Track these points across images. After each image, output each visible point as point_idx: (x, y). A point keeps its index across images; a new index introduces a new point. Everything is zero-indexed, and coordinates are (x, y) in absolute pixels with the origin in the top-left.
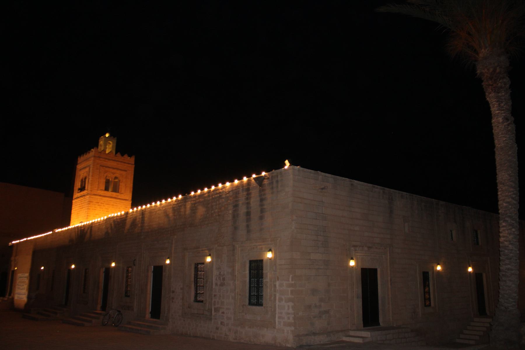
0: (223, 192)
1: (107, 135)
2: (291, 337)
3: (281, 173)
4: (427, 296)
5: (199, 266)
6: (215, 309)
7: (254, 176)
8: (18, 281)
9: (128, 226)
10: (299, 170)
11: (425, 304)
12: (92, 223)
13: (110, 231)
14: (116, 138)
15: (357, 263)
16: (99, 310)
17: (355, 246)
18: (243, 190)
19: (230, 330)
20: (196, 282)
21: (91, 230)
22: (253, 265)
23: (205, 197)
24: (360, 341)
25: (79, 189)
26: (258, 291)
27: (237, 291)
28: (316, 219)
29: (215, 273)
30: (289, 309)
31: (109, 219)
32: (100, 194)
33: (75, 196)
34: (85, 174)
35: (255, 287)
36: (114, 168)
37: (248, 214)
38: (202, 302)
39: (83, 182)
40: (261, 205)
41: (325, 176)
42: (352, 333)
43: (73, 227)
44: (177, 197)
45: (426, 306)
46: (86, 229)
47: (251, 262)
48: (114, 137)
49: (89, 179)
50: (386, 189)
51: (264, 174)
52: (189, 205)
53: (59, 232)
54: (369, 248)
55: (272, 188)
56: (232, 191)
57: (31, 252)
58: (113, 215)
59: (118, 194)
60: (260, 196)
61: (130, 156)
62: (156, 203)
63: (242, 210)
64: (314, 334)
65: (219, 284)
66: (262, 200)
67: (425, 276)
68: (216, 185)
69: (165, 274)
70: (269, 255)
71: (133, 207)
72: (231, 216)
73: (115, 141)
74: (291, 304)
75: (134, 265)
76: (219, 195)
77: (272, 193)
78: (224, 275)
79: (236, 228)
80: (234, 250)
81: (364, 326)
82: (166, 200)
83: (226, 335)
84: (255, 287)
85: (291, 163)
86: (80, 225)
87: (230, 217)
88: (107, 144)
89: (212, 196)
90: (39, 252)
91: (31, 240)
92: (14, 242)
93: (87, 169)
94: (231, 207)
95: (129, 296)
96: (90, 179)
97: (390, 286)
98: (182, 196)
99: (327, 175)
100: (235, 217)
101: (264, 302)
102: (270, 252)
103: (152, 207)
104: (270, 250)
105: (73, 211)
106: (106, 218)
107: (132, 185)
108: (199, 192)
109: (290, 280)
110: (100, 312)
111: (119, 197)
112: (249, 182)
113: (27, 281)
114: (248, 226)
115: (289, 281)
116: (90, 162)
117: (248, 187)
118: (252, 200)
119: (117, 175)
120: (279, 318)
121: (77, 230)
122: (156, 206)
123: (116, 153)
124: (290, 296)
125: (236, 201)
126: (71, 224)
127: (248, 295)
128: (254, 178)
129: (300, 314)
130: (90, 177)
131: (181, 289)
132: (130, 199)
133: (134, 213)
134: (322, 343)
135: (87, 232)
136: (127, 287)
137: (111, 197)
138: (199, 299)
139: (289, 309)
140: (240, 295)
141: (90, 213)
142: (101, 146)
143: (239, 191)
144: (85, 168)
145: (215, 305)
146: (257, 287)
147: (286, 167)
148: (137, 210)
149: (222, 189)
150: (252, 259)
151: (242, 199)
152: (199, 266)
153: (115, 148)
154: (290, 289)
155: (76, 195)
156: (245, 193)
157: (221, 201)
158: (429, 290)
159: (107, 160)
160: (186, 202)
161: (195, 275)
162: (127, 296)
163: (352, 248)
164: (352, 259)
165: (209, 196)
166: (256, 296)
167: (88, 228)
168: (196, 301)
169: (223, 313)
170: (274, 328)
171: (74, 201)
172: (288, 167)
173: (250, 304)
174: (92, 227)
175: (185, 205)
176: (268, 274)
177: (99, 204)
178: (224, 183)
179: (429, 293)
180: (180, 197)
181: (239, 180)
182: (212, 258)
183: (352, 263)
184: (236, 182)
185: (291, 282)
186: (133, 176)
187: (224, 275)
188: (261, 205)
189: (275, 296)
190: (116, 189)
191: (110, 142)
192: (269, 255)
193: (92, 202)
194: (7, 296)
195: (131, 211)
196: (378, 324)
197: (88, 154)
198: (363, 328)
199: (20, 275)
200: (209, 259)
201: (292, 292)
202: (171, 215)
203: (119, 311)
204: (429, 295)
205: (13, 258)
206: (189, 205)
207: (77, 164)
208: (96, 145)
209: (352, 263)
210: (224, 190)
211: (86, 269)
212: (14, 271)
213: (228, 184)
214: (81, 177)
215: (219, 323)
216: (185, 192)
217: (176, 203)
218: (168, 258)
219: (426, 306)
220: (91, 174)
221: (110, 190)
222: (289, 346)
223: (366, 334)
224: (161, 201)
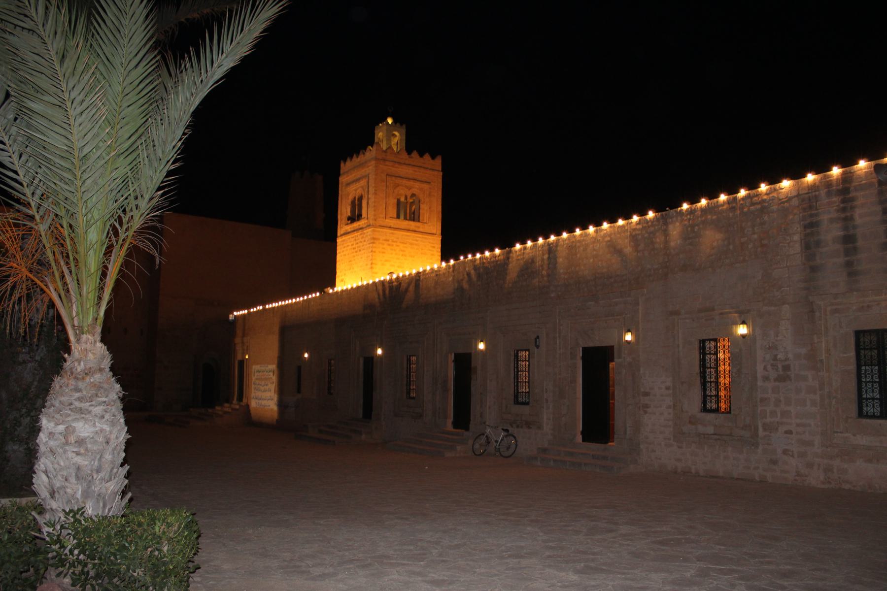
0: (773, 199)
6: (764, 425)
8: (254, 378)
12: (418, 273)
14: (404, 126)
18: (829, 194)
25: (349, 218)
32: (389, 225)
34: (359, 192)
36: (409, 179)
37: (849, 240)
46: (404, 285)
48: (401, 125)
56: (798, 195)
57: (276, 329)
59: (417, 224)
72: (797, 248)
73: (404, 131)
76: (763, 206)
80: (812, 311)
83: (798, 474)
88: (389, 135)
90: (291, 331)
93: (363, 183)
100: (810, 246)
111: (421, 230)
118: (857, 212)
119: (415, 191)
121: (380, 288)
125: (844, 210)
132: (440, 232)
133: (528, 251)
135: (407, 290)
137: (408, 230)
144: (358, 180)
149: (767, 194)
155: (342, 228)
159: (397, 165)
160: (666, 224)
165: (733, 209)
167: (409, 284)
177: (390, 242)
190: (414, 217)
191: (396, 133)
193: (378, 239)
194: (235, 401)
199: (256, 367)
202: (628, 250)
203: (507, 431)
205: (238, 340)
206: (675, 230)
208: (369, 140)
213: (786, 184)
214: (351, 197)
216: (666, 202)
220: (372, 190)
221: (402, 217)
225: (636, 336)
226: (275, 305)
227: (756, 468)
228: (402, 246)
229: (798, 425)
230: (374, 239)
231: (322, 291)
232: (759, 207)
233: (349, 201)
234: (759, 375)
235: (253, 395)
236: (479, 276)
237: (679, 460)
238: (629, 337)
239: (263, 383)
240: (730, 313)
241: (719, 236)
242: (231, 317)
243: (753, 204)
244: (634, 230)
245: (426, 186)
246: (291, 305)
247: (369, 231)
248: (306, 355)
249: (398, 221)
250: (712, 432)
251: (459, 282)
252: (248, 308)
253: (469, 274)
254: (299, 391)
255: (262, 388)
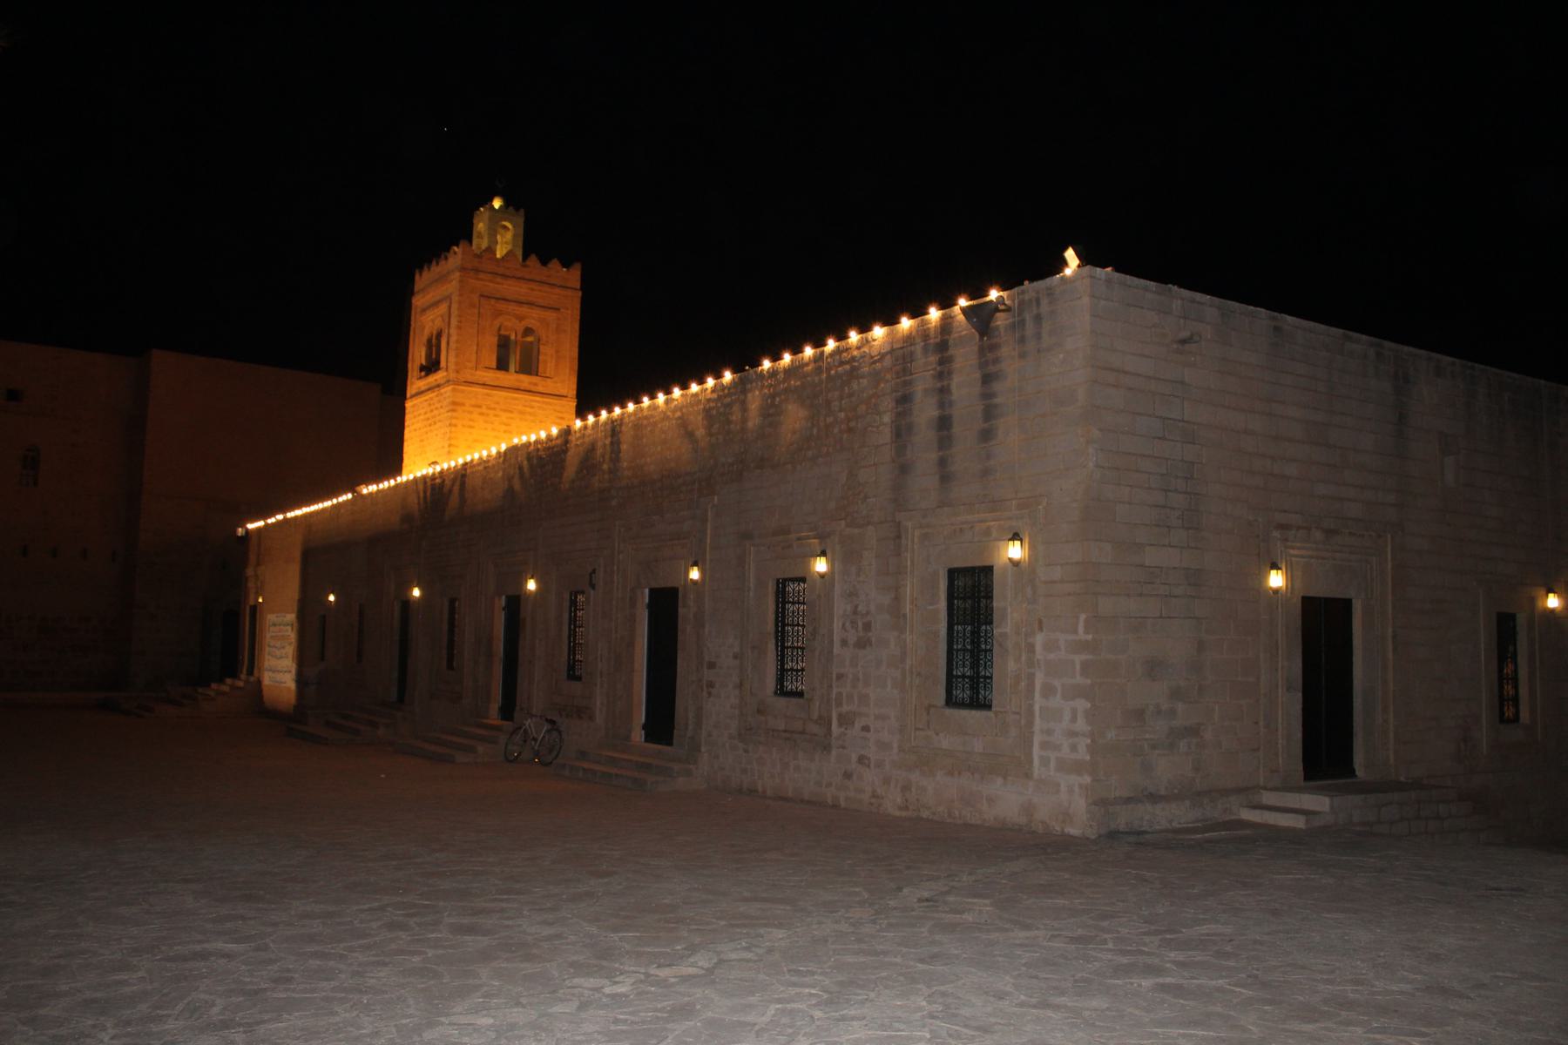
1: (497, 203)
2: (1080, 805)
3: (1050, 292)
4: (1509, 689)
5: (787, 591)
6: (840, 716)
7: (963, 302)
9: (571, 470)
10: (1109, 281)
11: (1502, 713)
13: (517, 485)
14: (522, 211)
15: (1290, 578)
16: (494, 716)
17: (1282, 527)
18: (925, 349)
19: (886, 781)
20: (780, 636)
21: (463, 484)
22: (960, 583)
23: (805, 376)
24: (1298, 822)
25: (422, 368)
26: (975, 665)
27: (908, 662)
28: (1163, 438)
29: (840, 607)
30: (1074, 719)
31: (513, 450)
33: (410, 390)
34: (438, 323)
35: (965, 650)
37: (944, 423)
38: (800, 694)
39: (433, 346)
40: (987, 396)
41: (1193, 301)
42: (1268, 798)
43: (411, 477)
44: (718, 376)
45: (1502, 719)
47: (953, 574)
49: (449, 336)
50: (1387, 344)
51: (994, 294)
52: (755, 400)
53: (370, 494)
54: (1330, 532)
55: (1022, 340)
56: (892, 351)
57: (297, 554)
58: (524, 439)
59: (534, 379)
60: (983, 365)
61: (566, 264)
62: (653, 397)
63: (925, 412)
64: (1154, 798)
65: (852, 639)
66: (987, 379)
67: (1505, 628)
68: (841, 336)
69: (686, 612)
70: (1015, 551)
71: (581, 413)
73: (521, 221)
74: (1082, 705)
75: (593, 586)
76: (849, 366)
77: (1022, 356)
78: (868, 613)
79: (904, 469)
80: (899, 537)
81: (1307, 778)
82: (685, 387)
83: (874, 795)
84: (965, 650)
85: (1085, 260)
86: (430, 471)
87: (886, 435)
88: (498, 230)
89: (828, 370)
90: (322, 554)
91: (296, 518)
92: (250, 526)
93: (443, 308)
94: (887, 403)
95: (579, 678)
96: (453, 339)
97: (1390, 655)
98: (734, 372)
99: (1198, 296)
100: (901, 432)
101: (996, 698)
102: (1018, 543)
103: (642, 409)
104: (1015, 537)
105: (408, 434)
106: (503, 447)
107: (576, 350)
108: (787, 358)
109: (1081, 629)
110: (499, 722)
111: (541, 389)
112: (946, 322)
113: (292, 635)
114: (942, 462)
115: (1075, 632)
116: (451, 287)
117: (942, 341)
118: (956, 380)
119: (531, 323)
120: (1045, 745)
121: (421, 487)
122: (653, 408)
123: (526, 256)
124: (1079, 679)
126: (405, 470)
127: (944, 677)
128: (964, 310)
129: (1111, 734)
130: (453, 331)
131: (735, 657)
133: (589, 431)
134: (1175, 825)
136: (572, 651)
137: (517, 390)
138: (789, 686)
139: (1074, 719)
140: (919, 674)
141: (460, 432)
142: (480, 236)
143: (912, 353)
144: (436, 304)
145: (839, 704)
146: (972, 651)
147: (1068, 272)
148: (596, 423)
149: (858, 348)
150: (956, 565)
151: (923, 381)
152: (791, 587)
153: (521, 243)
154: (1078, 659)
155: (415, 384)
156: (933, 358)
157: (855, 386)
158: (1516, 671)
159: (499, 279)
160: (744, 392)
161: (777, 612)
162: (573, 675)
163: (1276, 534)
164: (1275, 566)
165: (818, 370)
166: (969, 677)
167: (454, 481)
168: (781, 691)
169: (866, 729)
170: (1028, 776)
171: (409, 405)
172: (1075, 273)
173: (951, 702)
174: (464, 476)
175: (743, 403)
176: (1010, 613)
177: (484, 410)
178: (864, 328)
179: (1515, 680)
180: (728, 376)
181: (913, 316)
182: (831, 563)
183: (1276, 580)
184: (906, 323)
185: (1082, 635)
186: (578, 306)
187: (868, 613)
188: (987, 396)
189: (1031, 677)
190: (529, 366)
192: (1015, 551)
194: (243, 676)
195: (578, 424)
196: (1352, 773)
197: (443, 262)
198: (1302, 783)
200: (821, 566)
201: (1085, 667)
202: (700, 432)
203: (552, 722)
204: (1516, 688)
205: (250, 572)
206: (755, 400)
207: (412, 294)
209: (1276, 580)
210: (866, 349)
211: (452, 602)
212: (255, 609)
213: (879, 332)
215: (854, 757)
216: (744, 361)
217: (715, 396)
218: (695, 564)
219: (1502, 719)
220: (454, 322)
221: (512, 367)
222: (1074, 831)
223: (1318, 802)
224: (668, 392)
225: (703, 572)
226: (298, 512)
227: (829, 785)
228: (504, 416)
229: (877, 717)
230: (454, 403)
231: (353, 491)
232: (848, 367)
233: (425, 339)
234: (836, 638)
235: (266, 664)
236: (531, 466)
237: (744, 771)
238: (695, 574)
239: (278, 644)
240: (808, 537)
241: (802, 413)
242: (240, 531)
243: (842, 363)
244: (709, 400)
245: (551, 316)
246: (324, 510)
247: (447, 390)
248: (332, 598)
249: (501, 375)
250: (782, 727)
251: (510, 479)
252: (264, 518)
253: (521, 468)
254: (322, 659)
255: (278, 653)
